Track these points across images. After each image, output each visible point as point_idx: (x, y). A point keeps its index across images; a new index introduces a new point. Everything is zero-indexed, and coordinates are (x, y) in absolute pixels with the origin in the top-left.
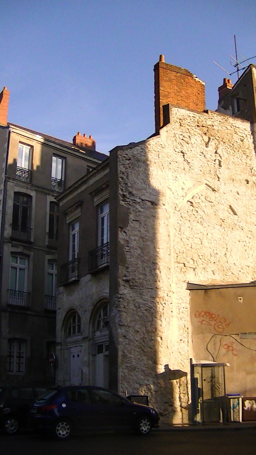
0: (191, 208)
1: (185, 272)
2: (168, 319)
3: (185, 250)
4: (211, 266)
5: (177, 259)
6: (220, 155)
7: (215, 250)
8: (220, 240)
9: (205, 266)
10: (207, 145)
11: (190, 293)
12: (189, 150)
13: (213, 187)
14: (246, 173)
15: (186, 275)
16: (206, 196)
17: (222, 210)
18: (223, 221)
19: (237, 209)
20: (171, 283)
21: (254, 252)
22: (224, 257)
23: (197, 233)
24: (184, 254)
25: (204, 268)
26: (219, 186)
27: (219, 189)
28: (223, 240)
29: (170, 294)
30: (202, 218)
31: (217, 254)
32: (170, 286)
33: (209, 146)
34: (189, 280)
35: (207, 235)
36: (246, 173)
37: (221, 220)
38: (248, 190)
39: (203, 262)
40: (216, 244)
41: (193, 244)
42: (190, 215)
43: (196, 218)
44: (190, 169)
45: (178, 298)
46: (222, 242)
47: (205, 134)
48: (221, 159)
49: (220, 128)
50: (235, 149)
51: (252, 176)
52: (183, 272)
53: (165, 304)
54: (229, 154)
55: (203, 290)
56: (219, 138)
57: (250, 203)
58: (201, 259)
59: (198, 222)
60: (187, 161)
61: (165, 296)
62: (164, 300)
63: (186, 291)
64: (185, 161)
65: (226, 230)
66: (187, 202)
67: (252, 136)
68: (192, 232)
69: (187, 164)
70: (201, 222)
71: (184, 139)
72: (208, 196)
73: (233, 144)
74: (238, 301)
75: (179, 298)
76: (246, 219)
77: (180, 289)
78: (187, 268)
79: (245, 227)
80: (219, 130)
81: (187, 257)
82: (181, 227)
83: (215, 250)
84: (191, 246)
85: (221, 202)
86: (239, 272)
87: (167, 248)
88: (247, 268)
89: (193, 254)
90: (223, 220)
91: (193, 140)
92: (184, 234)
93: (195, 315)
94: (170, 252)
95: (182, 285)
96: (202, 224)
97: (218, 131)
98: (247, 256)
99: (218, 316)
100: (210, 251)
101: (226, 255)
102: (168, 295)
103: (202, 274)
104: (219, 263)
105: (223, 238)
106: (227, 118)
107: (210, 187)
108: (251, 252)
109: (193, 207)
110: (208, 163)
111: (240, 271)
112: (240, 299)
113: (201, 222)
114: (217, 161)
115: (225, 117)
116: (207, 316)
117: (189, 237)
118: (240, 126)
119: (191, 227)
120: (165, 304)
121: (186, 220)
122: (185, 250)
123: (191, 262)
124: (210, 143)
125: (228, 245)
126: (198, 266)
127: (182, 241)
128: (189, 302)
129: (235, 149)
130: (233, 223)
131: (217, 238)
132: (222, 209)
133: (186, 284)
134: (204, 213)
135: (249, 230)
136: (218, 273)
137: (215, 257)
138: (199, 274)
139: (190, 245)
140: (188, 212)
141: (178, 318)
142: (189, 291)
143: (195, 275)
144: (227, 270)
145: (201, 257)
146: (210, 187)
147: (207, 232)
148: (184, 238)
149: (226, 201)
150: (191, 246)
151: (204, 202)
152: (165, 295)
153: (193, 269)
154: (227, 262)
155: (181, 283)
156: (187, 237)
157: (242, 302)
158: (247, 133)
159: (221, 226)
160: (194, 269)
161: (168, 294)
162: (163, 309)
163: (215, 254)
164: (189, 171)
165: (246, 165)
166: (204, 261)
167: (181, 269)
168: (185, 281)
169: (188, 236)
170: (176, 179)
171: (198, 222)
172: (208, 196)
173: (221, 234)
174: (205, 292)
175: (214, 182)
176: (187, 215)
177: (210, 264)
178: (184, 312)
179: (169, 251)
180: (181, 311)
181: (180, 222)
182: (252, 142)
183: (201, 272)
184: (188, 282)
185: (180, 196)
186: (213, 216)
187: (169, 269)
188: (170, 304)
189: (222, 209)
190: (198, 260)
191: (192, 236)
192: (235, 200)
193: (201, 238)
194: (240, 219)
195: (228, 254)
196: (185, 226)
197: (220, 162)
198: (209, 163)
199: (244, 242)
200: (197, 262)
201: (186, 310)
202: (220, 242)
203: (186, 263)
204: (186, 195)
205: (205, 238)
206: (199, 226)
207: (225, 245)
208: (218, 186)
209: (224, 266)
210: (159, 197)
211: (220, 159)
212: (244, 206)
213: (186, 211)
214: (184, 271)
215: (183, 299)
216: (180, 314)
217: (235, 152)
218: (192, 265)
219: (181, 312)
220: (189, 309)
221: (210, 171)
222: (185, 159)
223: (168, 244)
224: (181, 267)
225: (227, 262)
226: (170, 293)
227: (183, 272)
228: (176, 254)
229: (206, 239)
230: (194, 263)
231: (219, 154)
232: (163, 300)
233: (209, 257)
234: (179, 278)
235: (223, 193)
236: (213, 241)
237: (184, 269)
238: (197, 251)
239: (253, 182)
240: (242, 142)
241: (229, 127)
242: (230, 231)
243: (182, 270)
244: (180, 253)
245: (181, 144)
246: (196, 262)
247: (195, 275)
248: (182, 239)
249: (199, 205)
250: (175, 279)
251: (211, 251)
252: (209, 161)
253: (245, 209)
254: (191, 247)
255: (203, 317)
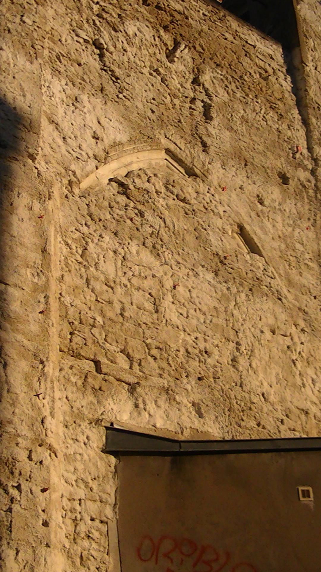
0: (122, 199)
1: (100, 389)
2: (30, 551)
3: (99, 319)
4: (189, 387)
5: (71, 341)
6: (206, 90)
7: (201, 339)
8: (215, 314)
9: (168, 382)
10: (170, 55)
11: (115, 467)
12: (119, 45)
13: (188, 161)
14: (280, 156)
15: (106, 403)
16: (168, 181)
17: (217, 230)
18: (221, 262)
19: (260, 238)
20: (46, 412)
21: (318, 373)
22: (232, 369)
23: (140, 275)
24: (95, 331)
25: (167, 391)
26: (207, 166)
27: (205, 173)
28: (223, 316)
29: (42, 453)
30: (155, 234)
31: (206, 352)
32: (43, 422)
33: (176, 59)
34: (113, 419)
35: (174, 288)
36: (280, 156)
37: (216, 260)
38: (288, 201)
39: (163, 369)
40: (202, 321)
41: (127, 306)
42: (118, 218)
43: (138, 229)
44: (121, 96)
45: (72, 478)
46: (221, 321)
47: (166, 28)
48: (211, 100)
49: (205, 28)
50: (247, 91)
51: (296, 168)
52: (93, 388)
53: (18, 488)
54: (232, 96)
55: (168, 459)
56: (203, 49)
57: (296, 233)
58: (155, 359)
59: (144, 244)
60: (112, 71)
61: (20, 458)
62: (17, 472)
63: (101, 458)
64: (105, 71)
65: (234, 290)
66: (108, 182)
67: (289, 78)
68: (127, 270)
69: (111, 82)
70: (154, 247)
71: (105, 15)
72: (174, 181)
73: (241, 77)
74: (299, 499)
75: (76, 481)
76: (287, 274)
77: (79, 448)
78: (107, 377)
79: (288, 295)
80: (202, 31)
81: (106, 340)
82: (87, 243)
83: (201, 339)
84: (123, 309)
85: (213, 207)
86: (279, 423)
87: (36, 289)
88: (303, 417)
89: (129, 338)
90: (222, 258)
91: (131, 28)
92: (97, 269)
93: (139, 550)
94: (47, 303)
95: (88, 432)
96: (158, 255)
97: (200, 33)
98: (299, 382)
99: (228, 555)
100: (184, 340)
101: (234, 363)
102: (34, 457)
103: (158, 407)
104: (215, 382)
105: (226, 311)
106: (222, 14)
107: (180, 161)
108: (310, 372)
109: (128, 198)
110: (172, 100)
111: (282, 422)
112: (306, 494)
113: (154, 247)
114: (199, 104)
115: (218, 9)
116: (182, 553)
117: (115, 282)
118: (258, 45)
119: (120, 250)
120: (18, 488)
121: (106, 229)
122: (99, 319)
123: (123, 362)
124: (178, 54)
125: (241, 335)
126: (146, 378)
127: (90, 287)
128: (112, 500)
129: (247, 91)
130: (250, 275)
131: (206, 305)
132: (218, 228)
133: (103, 431)
134: (163, 225)
135: (298, 305)
136: (212, 412)
137: (200, 361)
138: (151, 407)
139: (118, 307)
140: (111, 207)
141: (69, 556)
142: (113, 460)
143: (137, 406)
144: (243, 411)
145: (154, 352)
146: (180, 161)
147: (174, 282)
148: (97, 279)
149: (227, 208)
150: (123, 309)
151: (162, 195)
152: (22, 455)
153: (127, 387)
154: (239, 384)
155: (85, 424)
156: (107, 279)
157: (312, 505)
158: (274, 65)
159: (216, 275)
160: (132, 388)
161: (31, 451)
162: (10, 510)
163: (200, 351)
164: (117, 100)
165: (279, 135)
166: (164, 365)
167: (86, 377)
168: (98, 422)
169: (112, 276)
170: (77, 105)
171: (144, 244)
172: (174, 181)
173: (218, 297)
174: (173, 462)
175: (192, 150)
176: (109, 217)
177: (185, 381)
178: (96, 534)
179: (42, 300)
180: (82, 528)
181: (85, 229)
182: (289, 89)
183: (156, 401)
184: (112, 424)
185: (87, 154)
186: (190, 239)
187: (42, 362)
188: (37, 490)
189: (218, 228)
190: (146, 359)
191: (124, 280)
192: (253, 214)
193: (153, 294)
194: (271, 269)
195: (243, 362)
196: (100, 243)
197: (207, 108)
198: (176, 102)
199: (288, 339)
200: (142, 364)
201: (104, 528)
202: (215, 320)
203: (103, 360)
204: (105, 159)
205: (169, 298)
206: (147, 257)
207: (232, 333)
208: (204, 165)
209: (233, 397)
210: (16, 127)
211: (207, 100)
212: (279, 237)
213: (106, 204)
214: (97, 387)
215: (94, 485)
216: (79, 541)
217: (247, 95)
218: (122, 369)
219: (83, 535)
220: (113, 525)
221: (180, 121)
222: (104, 66)
223: (38, 274)
224: (85, 371)
225: (241, 386)
226: (39, 449)
227: (93, 388)
228: (66, 324)
229: (172, 300)
230: (131, 368)
231: (204, 87)
232: (12, 473)
233: (182, 358)
234: (77, 405)
235: (220, 186)
236: (192, 311)
237: (95, 378)
238: (141, 330)
239: (299, 183)
240: (265, 80)
241: (230, 37)
242: (243, 295)
243: (90, 380)
244: (81, 323)
245: (94, 24)
246: (140, 365)
247: (137, 406)
248: (92, 282)
249: (146, 196)
250: (61, 407)
251: (190, 340)
252: (175, 96)
253: (283, 246)
254: (122, 314)
255: (169, 557)
